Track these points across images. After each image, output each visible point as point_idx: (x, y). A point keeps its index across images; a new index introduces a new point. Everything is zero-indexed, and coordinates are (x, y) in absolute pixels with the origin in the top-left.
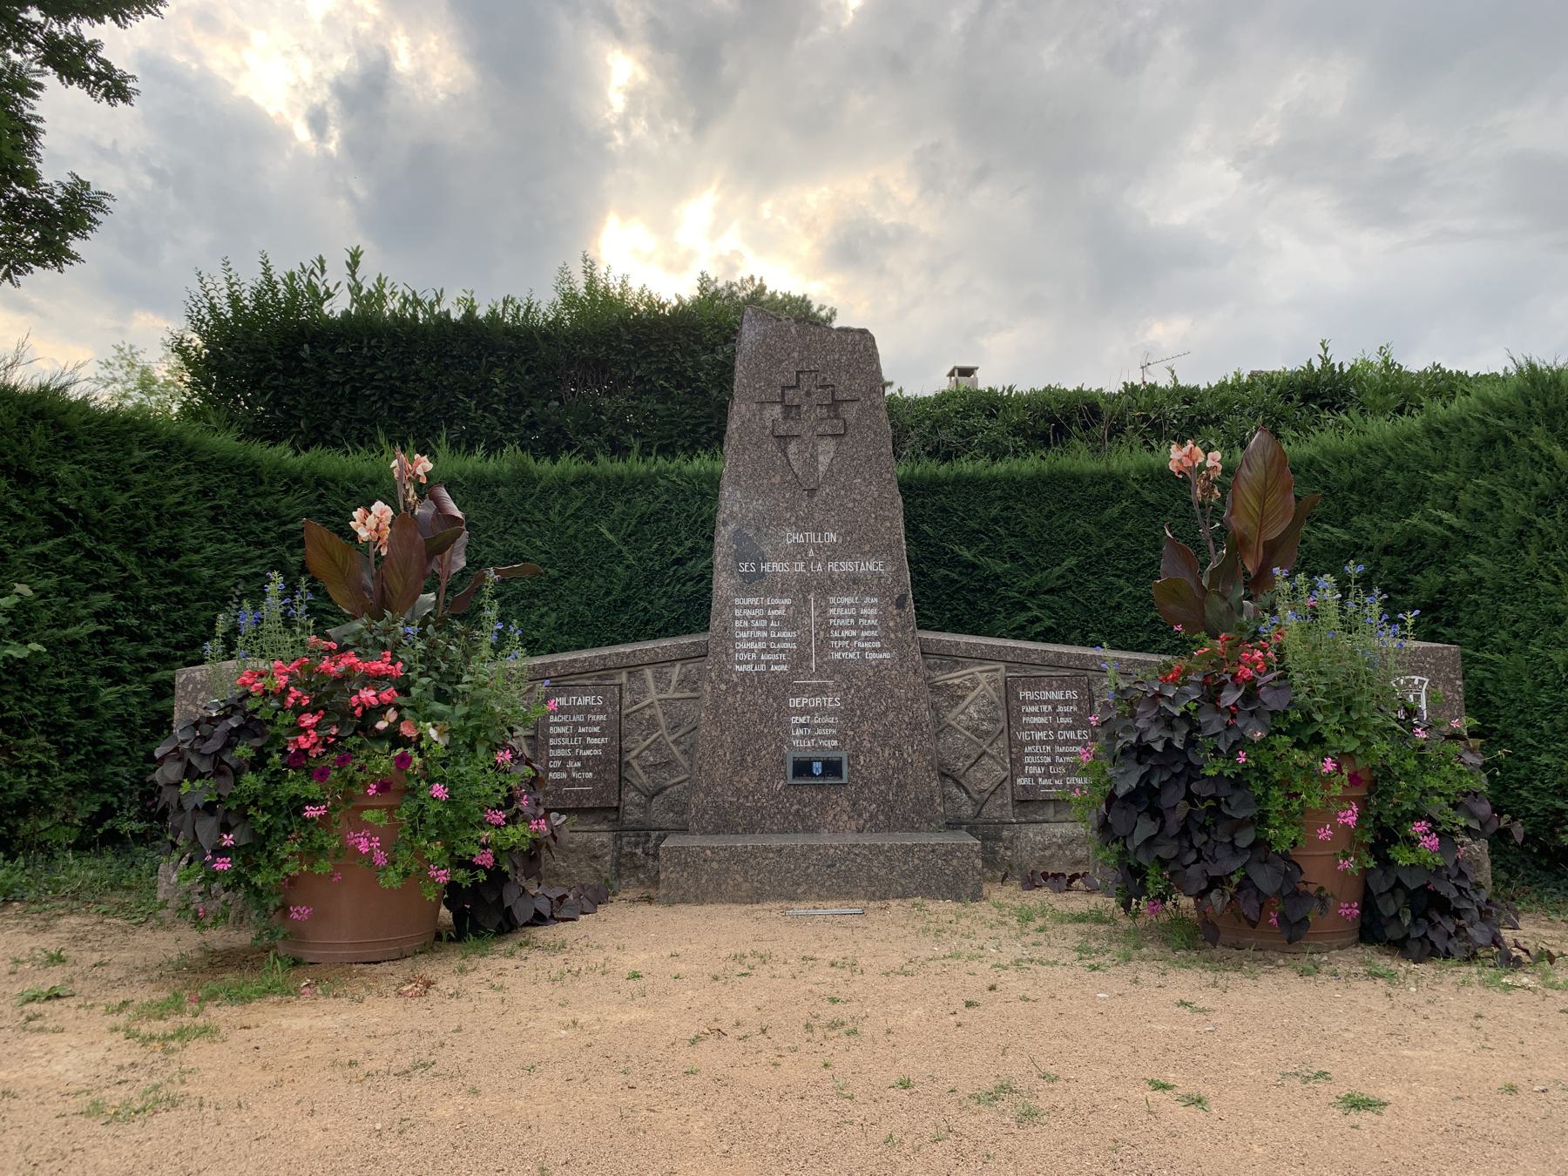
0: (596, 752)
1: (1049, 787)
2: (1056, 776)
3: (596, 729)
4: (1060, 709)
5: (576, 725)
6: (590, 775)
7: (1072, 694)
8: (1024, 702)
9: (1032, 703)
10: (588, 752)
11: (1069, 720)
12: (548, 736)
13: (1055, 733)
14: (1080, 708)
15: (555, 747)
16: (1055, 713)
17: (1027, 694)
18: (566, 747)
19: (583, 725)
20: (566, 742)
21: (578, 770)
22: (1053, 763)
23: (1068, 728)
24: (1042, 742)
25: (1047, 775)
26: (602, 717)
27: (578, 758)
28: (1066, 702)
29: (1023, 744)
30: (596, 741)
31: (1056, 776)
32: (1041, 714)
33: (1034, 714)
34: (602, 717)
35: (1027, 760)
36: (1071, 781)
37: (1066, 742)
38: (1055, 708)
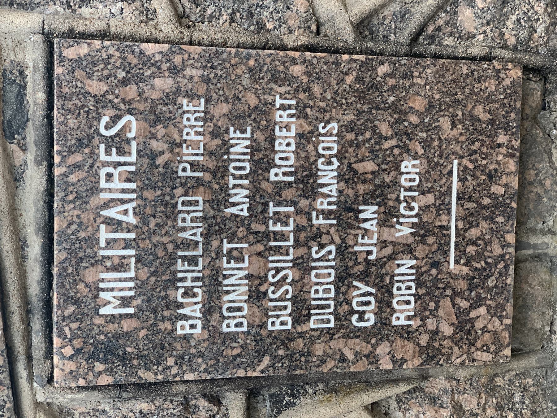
0: (329, 144)
3: (240, 143)
5: (217, 226)
6: (411, 169)
10: (328, 176)
12: (261, 342)
15: (302, 310)
18: (303, 265)
19: (220, 198)
20: (284, 264)
21: (388, 217)
26: (192, 110)
27: (346, 213)
30: (285, 145)
34: (192, 110)
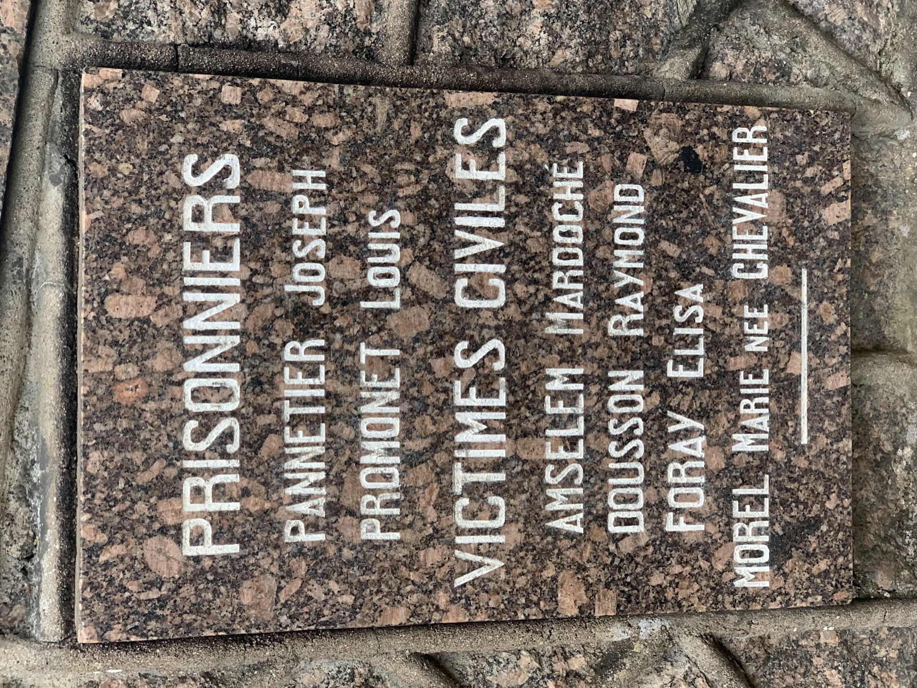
1: (784, 388)
2: (721, 344)
4: (308, 281)
7: (207, 193)
8: (253, 529)
9: (261, 464)
11: (386, 228)
13: (467, 328)
14: (310, 146)
16: (334, 321)
17: (196, 509)
22: (647, 357)
23: (433, 241)
24: (524, 415)
25: (717, 394)
28: (264, 237)
29: (538, 541)
31: (721, 344)
32: (339, 414)
33: (342, 461)
35: (627, 519)
36: (750, 248)
37: (525, 261)
38: (305, 320)
